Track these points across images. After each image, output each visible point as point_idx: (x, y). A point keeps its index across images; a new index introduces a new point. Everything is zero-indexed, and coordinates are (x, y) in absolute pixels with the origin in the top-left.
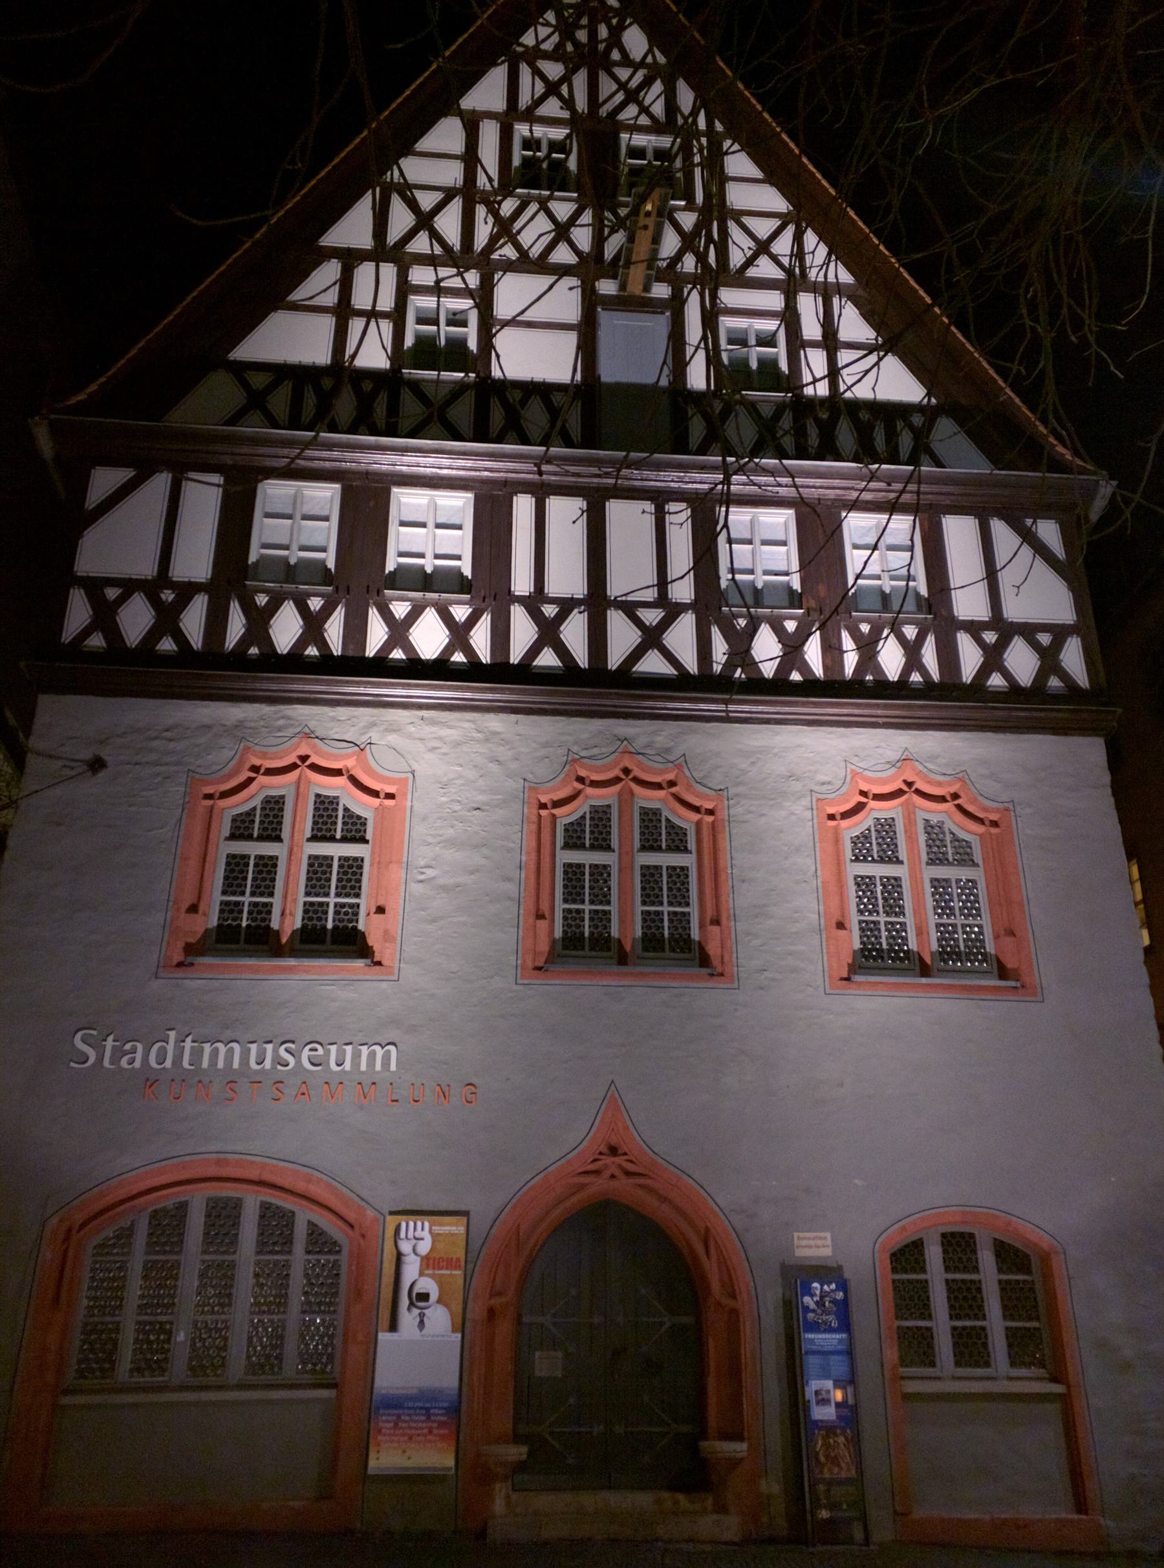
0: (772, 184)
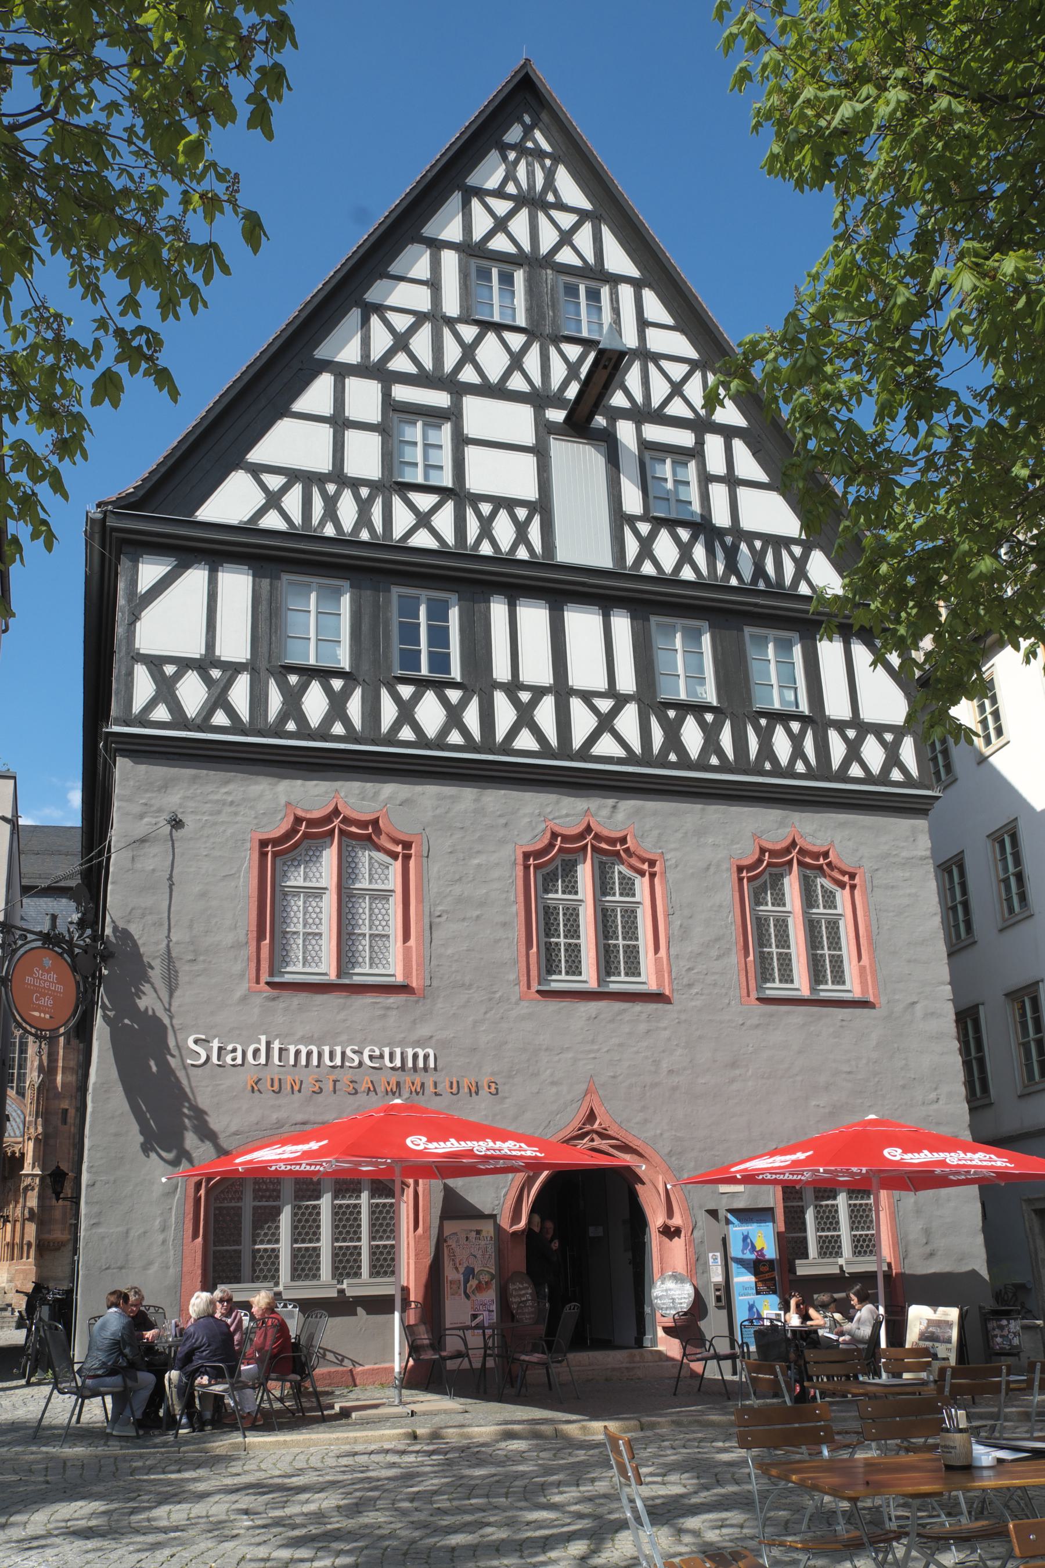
0: (683, 331)
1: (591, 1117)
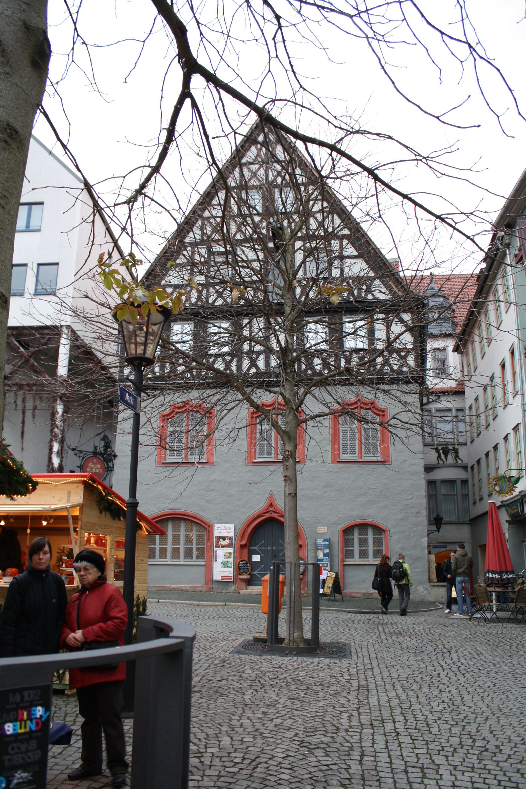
1: (271, 505)
